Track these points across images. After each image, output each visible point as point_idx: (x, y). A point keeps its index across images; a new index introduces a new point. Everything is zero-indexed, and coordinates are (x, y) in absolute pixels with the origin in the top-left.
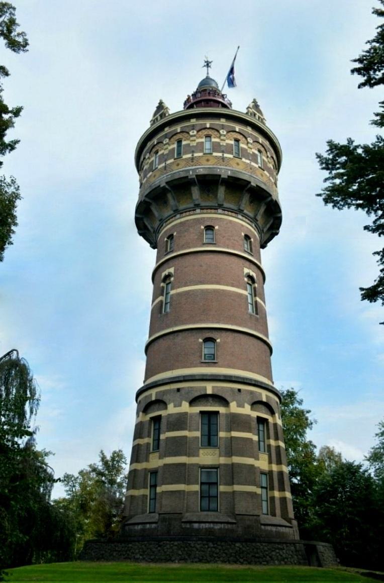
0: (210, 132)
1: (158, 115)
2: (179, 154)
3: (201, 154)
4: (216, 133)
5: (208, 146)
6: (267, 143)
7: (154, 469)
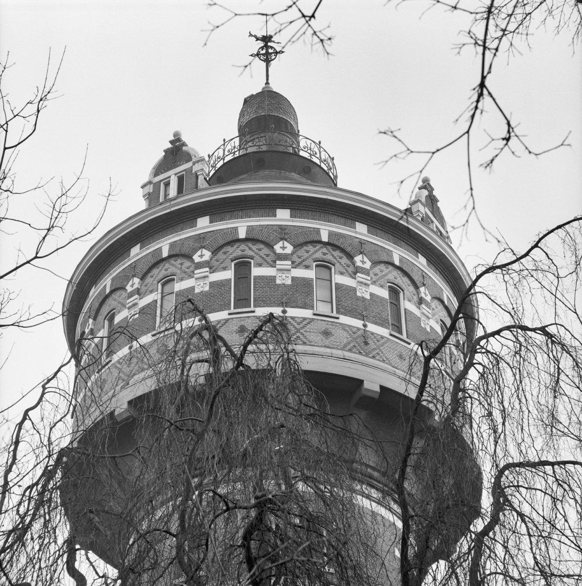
3: (307, 313)
4: (345, 260)
7: (332, 218)
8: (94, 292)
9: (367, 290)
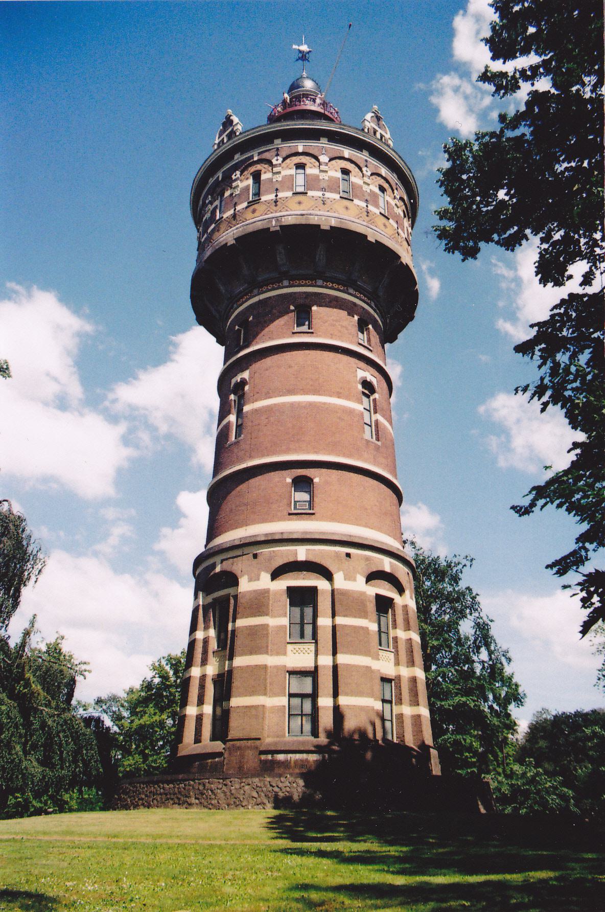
1: (224, 136)
2: (258, 194)
3: (289, 194)
5: (300, 180)
6: (393, 178)
8: (211, 181)
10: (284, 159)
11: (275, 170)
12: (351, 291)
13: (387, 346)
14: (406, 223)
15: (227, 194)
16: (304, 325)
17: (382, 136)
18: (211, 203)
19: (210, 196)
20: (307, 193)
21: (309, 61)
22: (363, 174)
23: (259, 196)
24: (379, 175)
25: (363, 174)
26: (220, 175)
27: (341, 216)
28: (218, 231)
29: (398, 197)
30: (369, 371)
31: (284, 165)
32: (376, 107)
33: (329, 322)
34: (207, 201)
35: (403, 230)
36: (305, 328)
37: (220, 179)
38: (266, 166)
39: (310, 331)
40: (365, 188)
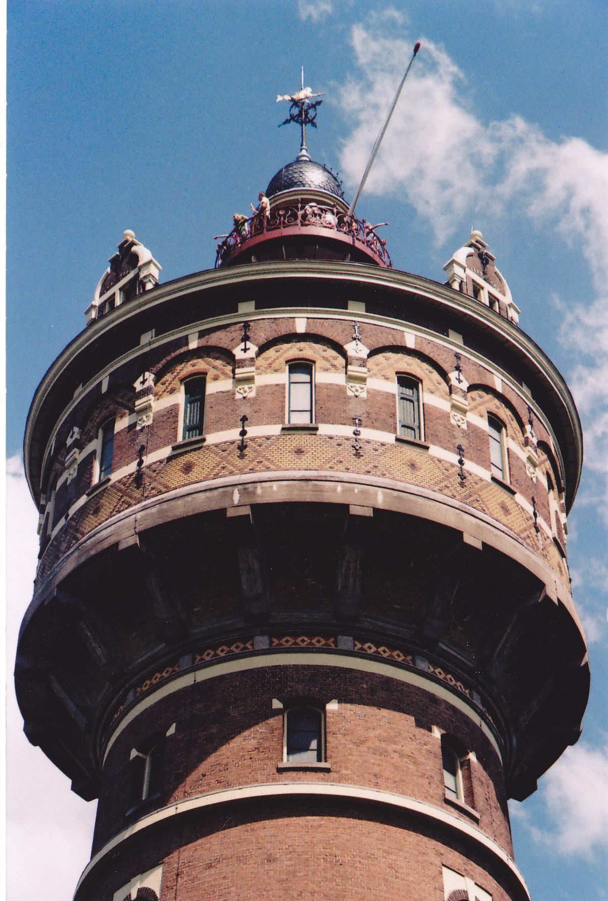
0: (308, 350)
1: (116, 289)
2: (197, 427)
3: (275, 430)
5: (300, 397)
6: (521, 396)
8: (80, 393)
9: (463, 418)
10: (263, 349)
11: (241, 372)
12: (423, 665)
13: (513, 804)
14: (554, 502)
15: (121, 425)
16: (306, 748)
17: (493, 299)
18: (79, 445)
19: (76, 429)
20: (316, 429)
21: (314, 125)
22: (450, 387)
23: (201, 434)
24: (489, 389)
25: (450, 387)
26: (104, 380)
27: (400, 485)
28: (96, 512)
29: (535, 441)
30: (472, 878)
31: (260, 361)
32: (478, 232)
33: (369, 744)
34: (69, 441)
35: (547, 520)
36: (308, 758)
37: (104, 389)
38: (218, 363)
39: (322, 765)
40: (456, 419)
